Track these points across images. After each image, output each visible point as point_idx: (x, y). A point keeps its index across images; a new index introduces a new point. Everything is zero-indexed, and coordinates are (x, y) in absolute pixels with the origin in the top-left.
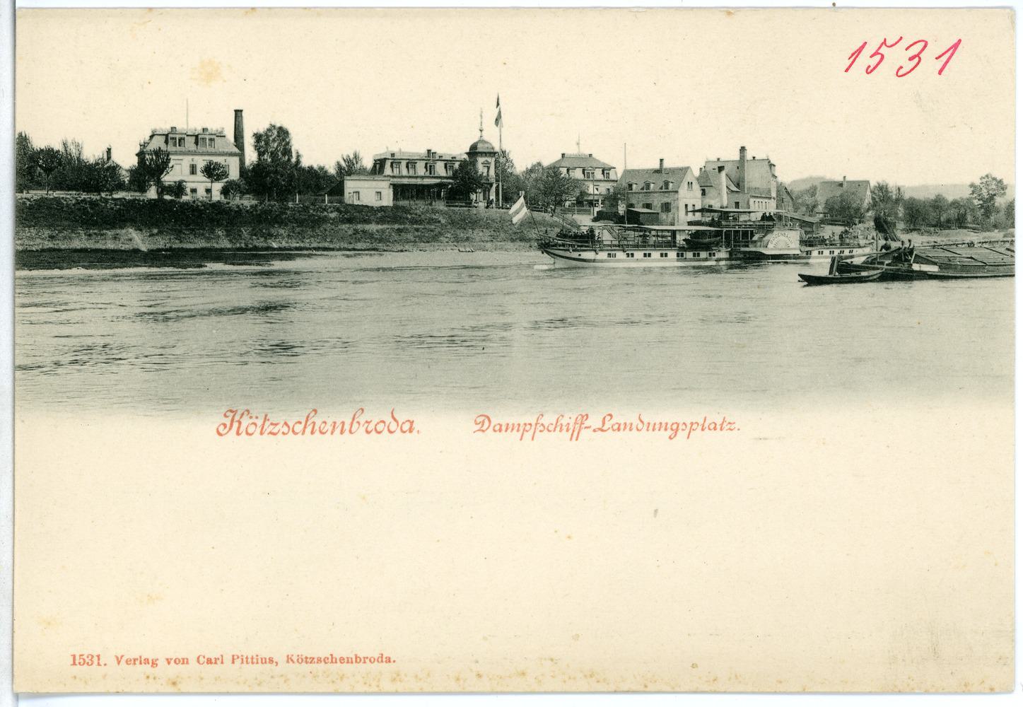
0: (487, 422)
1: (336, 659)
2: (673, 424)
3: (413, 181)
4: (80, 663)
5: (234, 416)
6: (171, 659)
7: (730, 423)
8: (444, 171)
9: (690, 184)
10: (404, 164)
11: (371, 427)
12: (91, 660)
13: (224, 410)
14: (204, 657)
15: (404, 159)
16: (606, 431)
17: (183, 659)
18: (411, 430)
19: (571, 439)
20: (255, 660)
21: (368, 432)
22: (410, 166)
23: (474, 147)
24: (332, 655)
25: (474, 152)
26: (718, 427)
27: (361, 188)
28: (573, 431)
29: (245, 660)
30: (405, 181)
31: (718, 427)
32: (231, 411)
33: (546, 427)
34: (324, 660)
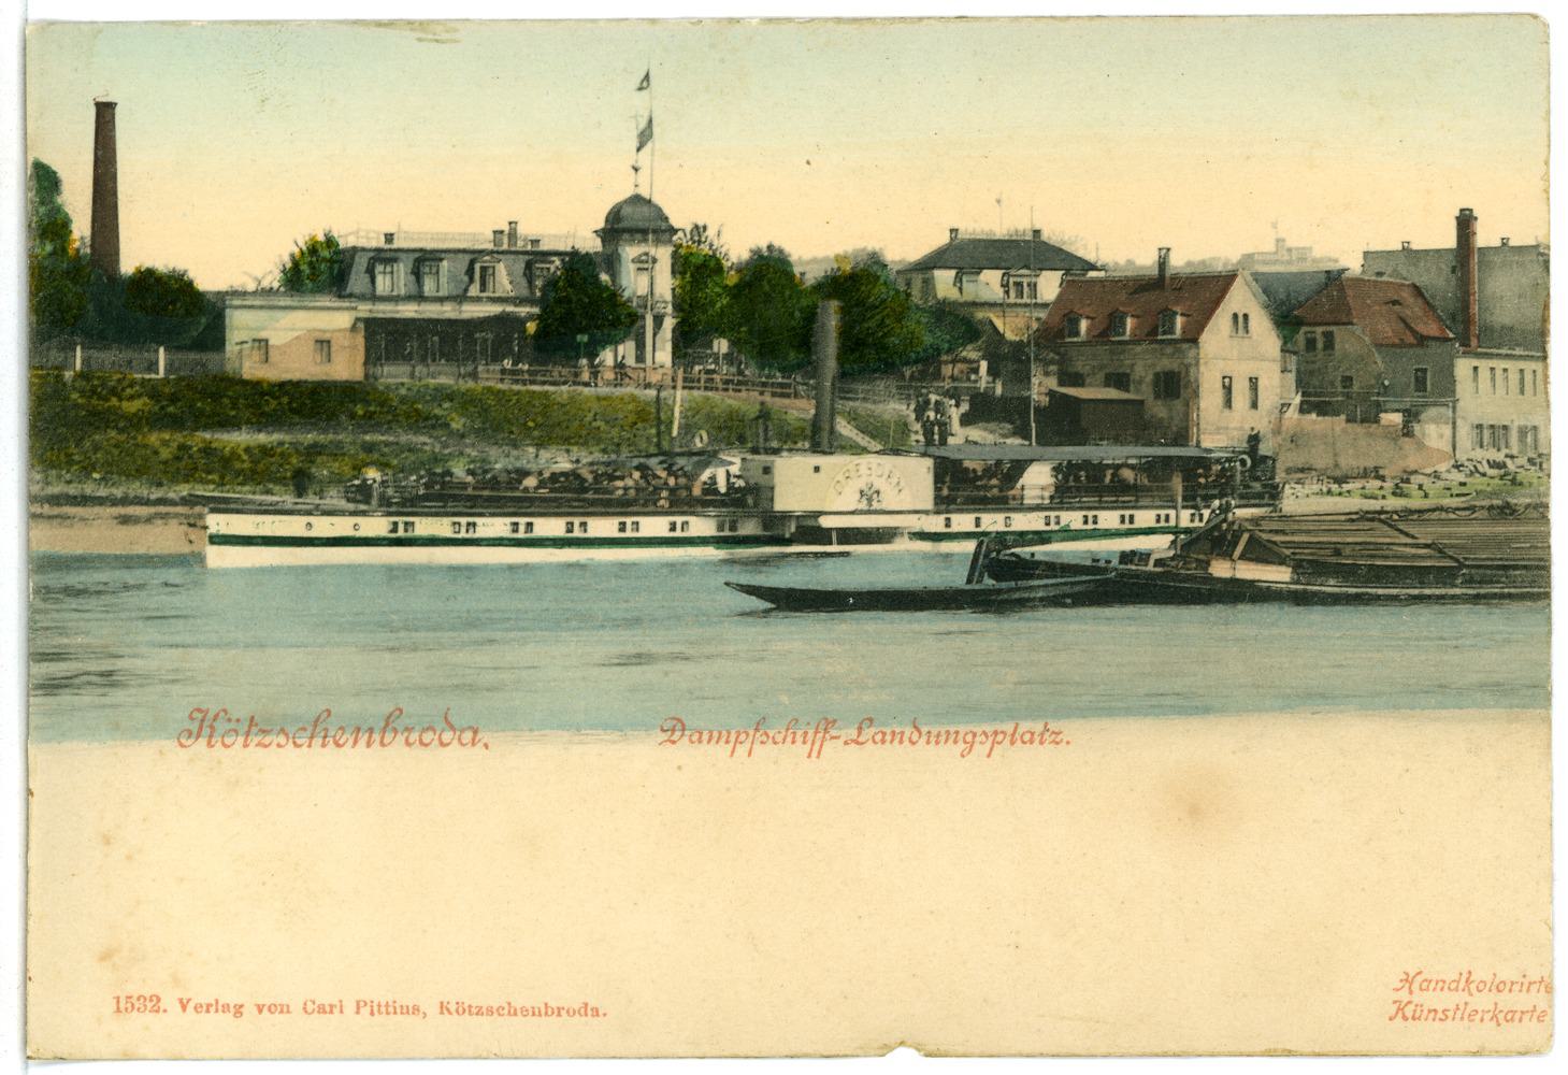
1: (515, 1010)
2: (966, 734)
4: (126, 1009)
6: (264, 1006)
7: (1053, 732)
9: (1241, 322)
14: (314, 1003)
16: (862, 743)
17: (281, 1006)
19: (809, 756)
20: (391, 1009)
21: (408, 743)
23: (615, 216)
24: (509, 1004)
25: (617, 228)
29: (375, 1009)
32: (199, 710)
34: (498, 1010)
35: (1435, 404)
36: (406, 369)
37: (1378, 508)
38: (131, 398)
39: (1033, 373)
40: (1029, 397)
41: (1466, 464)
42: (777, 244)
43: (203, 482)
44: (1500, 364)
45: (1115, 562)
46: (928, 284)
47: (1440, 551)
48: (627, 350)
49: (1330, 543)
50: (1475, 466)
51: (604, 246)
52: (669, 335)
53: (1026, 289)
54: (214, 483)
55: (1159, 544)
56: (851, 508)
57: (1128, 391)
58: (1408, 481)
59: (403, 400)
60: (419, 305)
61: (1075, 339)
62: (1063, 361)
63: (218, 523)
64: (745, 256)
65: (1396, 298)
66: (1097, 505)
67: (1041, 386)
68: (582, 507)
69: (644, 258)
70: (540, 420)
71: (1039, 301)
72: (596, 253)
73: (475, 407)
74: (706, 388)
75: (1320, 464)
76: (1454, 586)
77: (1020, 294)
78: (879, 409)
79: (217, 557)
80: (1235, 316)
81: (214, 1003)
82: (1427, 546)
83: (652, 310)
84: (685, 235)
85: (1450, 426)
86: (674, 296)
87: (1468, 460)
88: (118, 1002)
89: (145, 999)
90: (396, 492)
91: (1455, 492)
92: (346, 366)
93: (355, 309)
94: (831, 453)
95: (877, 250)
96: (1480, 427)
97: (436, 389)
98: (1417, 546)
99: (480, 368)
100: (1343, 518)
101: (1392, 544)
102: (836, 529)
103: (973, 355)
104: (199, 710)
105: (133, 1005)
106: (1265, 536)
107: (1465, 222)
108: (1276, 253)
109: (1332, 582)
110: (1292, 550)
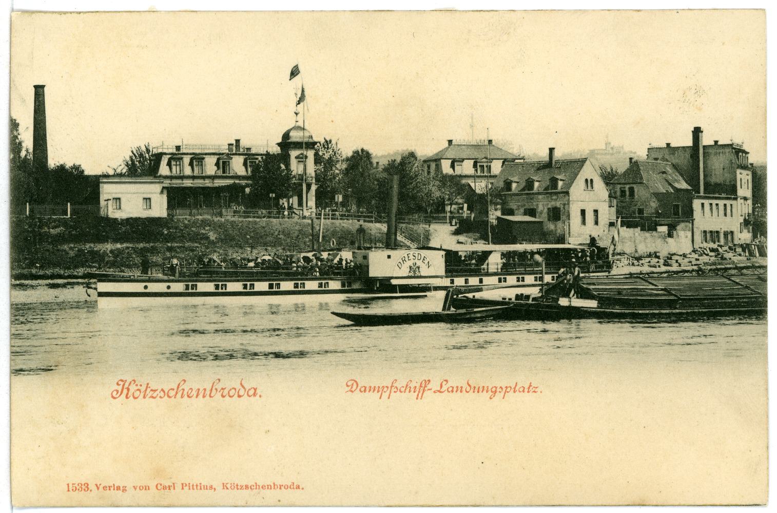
0: (355, 384)
1: (259, 486)
3: (199, 183)
4: (73, 490)
5: (124, 385)
6: (137, 486)
8: (243, 169)
9: (589, 183)
10: (187, 160)
11: (226, 392)
12: (87, 487)
13: (116, 381)
14: (161, 485)
15: (187, 154)
16: (443, 392)
17: (146, 486)
18: (255, 395)
19: (417, 399)
21: (223, 396)
22: (195, 163)
25: (286, 143)
26: (526, 390)
27: (122, 193)
28: (419, 392)
30: (188, 183)
31: (526, 390)
33: (166, 392)
35: (683, 221)
36: (188, 211)
37: (639, 272)
38: (55, 227)
39: (489, 209)
40: (488, 220)
41: (699, 250)
42: (365, 148)
43: (91, 267)
44: (714, 202)
45: (513, 300)
46: (438, 167)
47: (668, 292)
48: (294, 200)
49: (616, 289)
50: (703, 251)
51: (281, 151)
52: (314, 193)
53: (485, 169)
54: (96, 267)
55: (535, 292)
56: (406, 275)
57: (535, 217)
58: (671, 259)
59: (186, 226)
60: (193, 181)
61: (510, 193)
62: (503, 204)
63: (103, 287)
64: (350, 154)
65: (664, 170)
66: (524, 272)
67: (494, 215)
68: (277, 276)
69: (301, 156)
70: (252, 234)
71: (492, 174)
72: (278, 154)
73: (221, 229)
74: (332, 219)
75: (628, 251)
76: (676, 308)
77: (483, 171)
78: (415, 227)
79: (103, 302)
80: (586, 180)
81: (113, 486)
82: (662, 290)
83: (305, 181)
84: (321, 145)
85: (691, 232)
86: (316, 174)
87: (699, 248)
88: (68, 486)
89: (82, 485)
90: (187, 270)
91: (693, 263)
92: (159, 208)
93: (162, 182)
94: (396, 249)
95: (413, 151)
96: (705, 232)
97: (202, 221)
98: (657, 290)
99: (223, 210)
100: (622, 277)
101: (647, 289)
102: (399, 285)
103: (460, 201)
104: (122, 381)
105: (76, 487)
106: (585, 286)
107: (697, 132)
108: (606, 150)
109: (617, 307)
110: (598, 293)
